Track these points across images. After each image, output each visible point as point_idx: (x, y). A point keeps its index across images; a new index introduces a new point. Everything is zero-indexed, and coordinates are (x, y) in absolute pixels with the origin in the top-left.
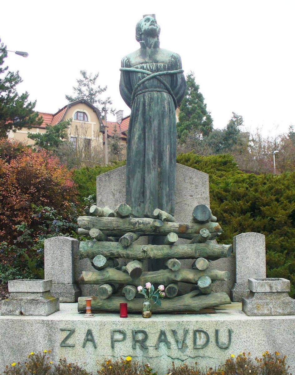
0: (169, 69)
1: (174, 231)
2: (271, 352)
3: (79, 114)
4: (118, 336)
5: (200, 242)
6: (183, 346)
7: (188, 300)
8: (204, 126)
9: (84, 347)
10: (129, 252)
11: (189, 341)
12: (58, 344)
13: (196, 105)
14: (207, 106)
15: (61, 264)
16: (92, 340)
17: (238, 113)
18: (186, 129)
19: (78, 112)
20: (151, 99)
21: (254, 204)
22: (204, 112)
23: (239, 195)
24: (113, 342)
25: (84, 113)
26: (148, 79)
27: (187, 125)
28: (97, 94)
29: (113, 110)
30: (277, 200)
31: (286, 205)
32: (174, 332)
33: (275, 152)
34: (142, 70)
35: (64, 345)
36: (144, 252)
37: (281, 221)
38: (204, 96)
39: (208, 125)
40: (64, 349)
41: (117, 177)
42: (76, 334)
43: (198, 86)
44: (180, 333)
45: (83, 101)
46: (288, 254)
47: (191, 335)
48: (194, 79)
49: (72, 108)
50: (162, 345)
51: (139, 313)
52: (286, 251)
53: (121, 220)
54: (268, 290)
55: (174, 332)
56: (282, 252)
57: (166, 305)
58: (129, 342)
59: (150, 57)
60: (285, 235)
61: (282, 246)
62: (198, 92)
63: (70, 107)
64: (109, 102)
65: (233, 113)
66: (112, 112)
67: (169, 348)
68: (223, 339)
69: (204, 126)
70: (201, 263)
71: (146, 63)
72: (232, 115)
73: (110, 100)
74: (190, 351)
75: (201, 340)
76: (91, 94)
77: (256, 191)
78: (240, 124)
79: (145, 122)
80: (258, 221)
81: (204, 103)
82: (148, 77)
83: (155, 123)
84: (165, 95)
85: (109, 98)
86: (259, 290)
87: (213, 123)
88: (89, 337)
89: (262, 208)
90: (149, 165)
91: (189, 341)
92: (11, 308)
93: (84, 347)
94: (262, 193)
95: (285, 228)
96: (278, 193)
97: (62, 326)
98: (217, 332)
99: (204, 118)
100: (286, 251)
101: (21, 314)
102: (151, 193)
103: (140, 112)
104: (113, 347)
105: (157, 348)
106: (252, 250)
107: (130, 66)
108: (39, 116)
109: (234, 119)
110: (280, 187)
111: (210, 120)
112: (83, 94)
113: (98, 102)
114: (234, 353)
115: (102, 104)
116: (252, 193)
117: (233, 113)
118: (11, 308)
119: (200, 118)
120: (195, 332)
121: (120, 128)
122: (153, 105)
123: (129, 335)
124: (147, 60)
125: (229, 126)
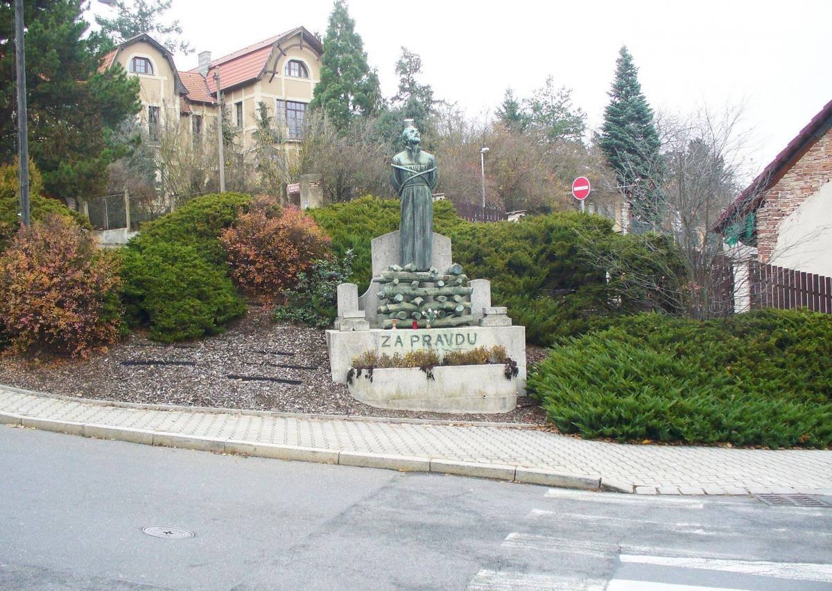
0: (428, 169)
1: (442, 280)
2: (498, 345)
3: (138, 61)
4: (415, 339)
5: (455, 286)
6: (450, 343)
7: (449, 319)
8: (365, 92)
9: (395, 346)
10: (416, 292)
11: (454, 340)
12: (380, 345)
13: (351, 56)
14: (368, 56)
15: (351, 303)
16: (400, 342)
17: (413, 49)
18: (334, 97)
19: (136, 58)
20: (418, 191)
21: (477, 254)
22: (364, 69)
23: (464, 246)
24: (412, 342)
25: (147, 60)
26: (415, 177)
27: (335, 91)
28: (156, 13)
29: (185, 44)
30: (496, 251)
31: (503, 256)
32: (445, 335)
33: (484, 149)
34: (410, 170)
35: (384, 345)
36: (426, 292)
37: (499, 269)
38: (364, 39)
39: (372, 91)
40: (384, 348)
41: (387, 240)
42: (391, 339)
43: (353, 21)
44: (449, 336)
45: (145, 39)
46: (505, 295)
47: (455, 336)
48: (347, 9)
49: (126, 51)
50: (439, 342)
51: (424, 327)
52: (503, 293)
53: (410, 273)
54: (495, 313)
55: (445, 335)
56: (501, 293)
57: (437, 322)
58: (421, 341)
59: (416, 161)
60: (503, 280)
61: (500, 289)
62: (354, 33)
63: (122, 50)
64: (176, 30)
65: (402, 48)
66: (184, 48)
67: (443, 344)
68: (472, 339)
69: (365, 92)
70: (457, 298)
71: (413, 164)
72: (402, 53)
73: (179, 25)
74: (454, 346)
75: (460, 339)
76: (143, 15)
77: (479, 243)
78: (416, 70)
79: (414, 207)
80: (481, 269)
81: (364, 51)
82: (415, 175)
83: (421, 208)
84: (426, 187)
85: (176, 23)
86: (490, 313)
87: (380, 86)
88: (399, 340)
89: (484, 258)
90: (417, 236)
91: (454, 340)
92: (347, 327)
93: (395, 346)
94: (483, 246)
95: (503, 274)
96: (497, 245)
97: (384, 335)
98: (468, 334)
99: (365, 78)
100: (503, 293)
101: (354, 330)
102: (419, 255)
103: (410, 200)
104: (412, 345)
105: (436, 344)
106: (481, 290)
107: (400, 165)
108: (799, 428)
109: (405, 61)
110: (499, 240)
111: (374, 80)
112: (127, 14)
113: (155, 30)
114: (478, 346)
115: (163, 32)
116: (475, 246)
117: (402, 48)
118: (347, 327)
119: (358, 77)
120: (457, 335)
121: (206, 84)
122: (419, 195)
123: (421, 337)
124: (414, 162)
125: (412, 103)
